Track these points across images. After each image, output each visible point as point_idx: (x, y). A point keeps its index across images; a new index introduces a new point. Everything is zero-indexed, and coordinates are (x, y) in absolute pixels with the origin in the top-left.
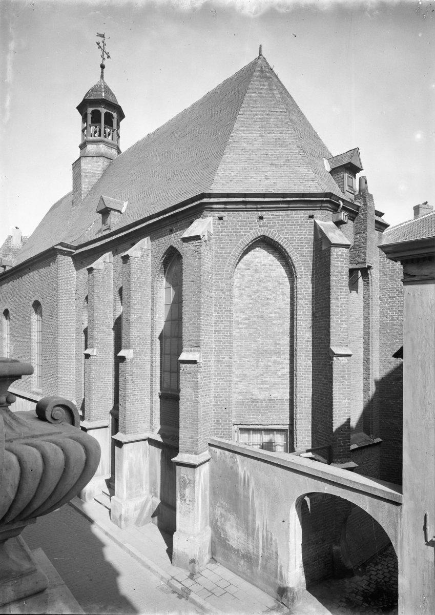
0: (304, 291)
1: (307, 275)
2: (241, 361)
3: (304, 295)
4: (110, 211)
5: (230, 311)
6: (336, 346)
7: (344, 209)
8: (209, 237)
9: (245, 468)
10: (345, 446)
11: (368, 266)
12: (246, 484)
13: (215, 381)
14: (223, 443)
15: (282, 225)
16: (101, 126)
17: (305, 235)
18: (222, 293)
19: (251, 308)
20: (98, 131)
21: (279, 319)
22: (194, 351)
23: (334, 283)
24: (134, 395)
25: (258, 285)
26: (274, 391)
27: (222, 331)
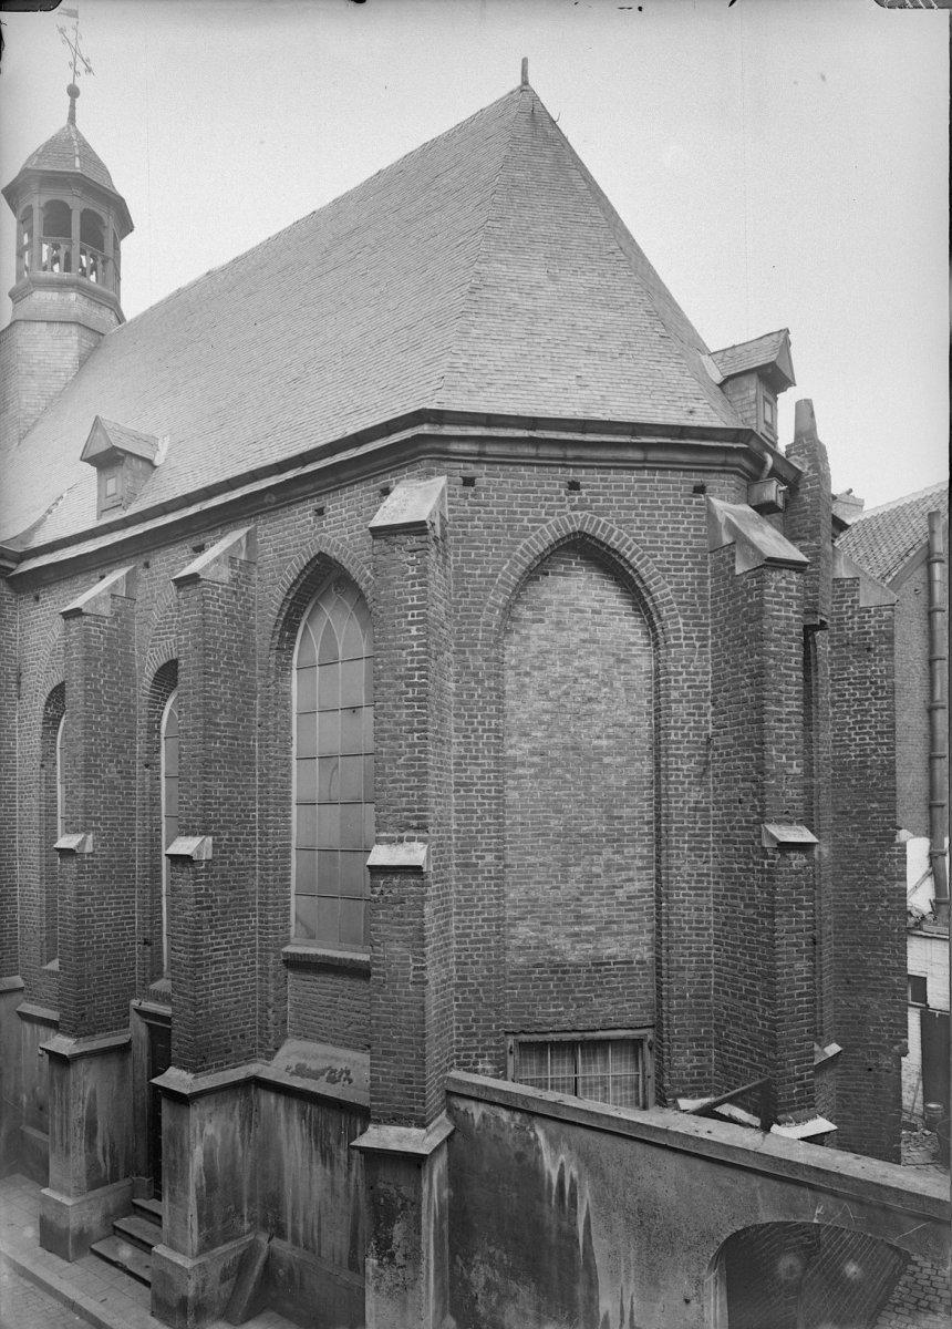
0: (685, 681)
1: (692, 638)
2: (523, 865)
3: (686, 690)
4: (123, 458)
5: (497, 731)
6: (779, 822)
7: (774, 473)
8: (443, 531)
9: (562, 1157)
10: (801, 1078)
11: (823, 623)
12: (566, 1199)
13: (460, 921)
14: (494, 1090)
15: (629, 508)
16: (70, 243)
17: (686, 536)
18: (476, 683)
19: (549, 724)
20: (62, 257)
21: (621, 754)
22: (411, 840)
23: (771, 661)
24: (215, 962)
25: (566, 663)
26: (608, 939)
27: (476, 784)
